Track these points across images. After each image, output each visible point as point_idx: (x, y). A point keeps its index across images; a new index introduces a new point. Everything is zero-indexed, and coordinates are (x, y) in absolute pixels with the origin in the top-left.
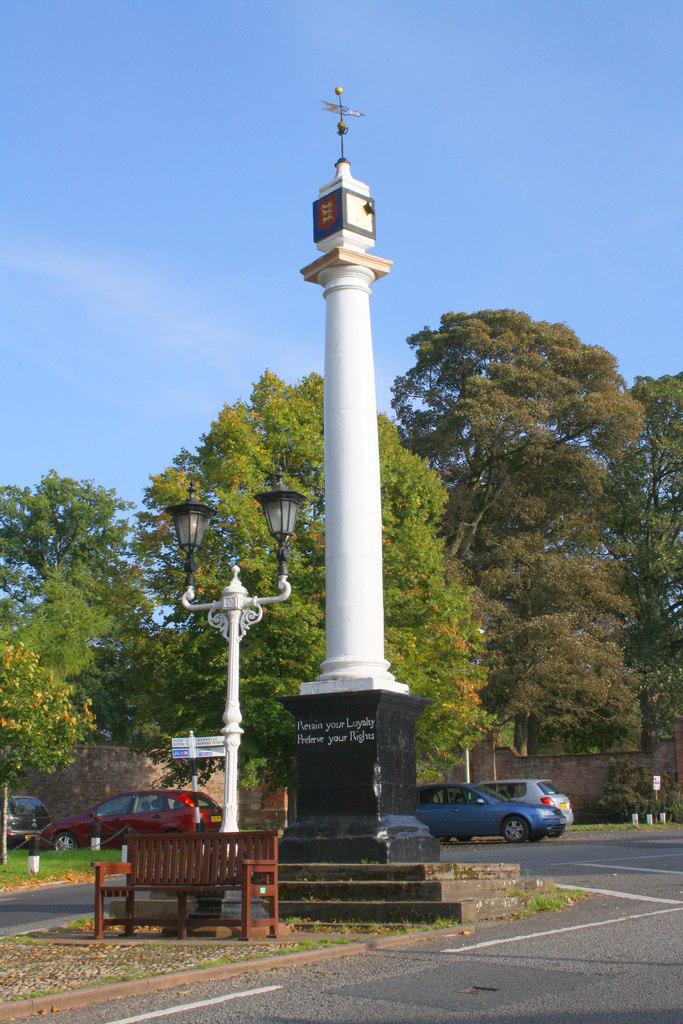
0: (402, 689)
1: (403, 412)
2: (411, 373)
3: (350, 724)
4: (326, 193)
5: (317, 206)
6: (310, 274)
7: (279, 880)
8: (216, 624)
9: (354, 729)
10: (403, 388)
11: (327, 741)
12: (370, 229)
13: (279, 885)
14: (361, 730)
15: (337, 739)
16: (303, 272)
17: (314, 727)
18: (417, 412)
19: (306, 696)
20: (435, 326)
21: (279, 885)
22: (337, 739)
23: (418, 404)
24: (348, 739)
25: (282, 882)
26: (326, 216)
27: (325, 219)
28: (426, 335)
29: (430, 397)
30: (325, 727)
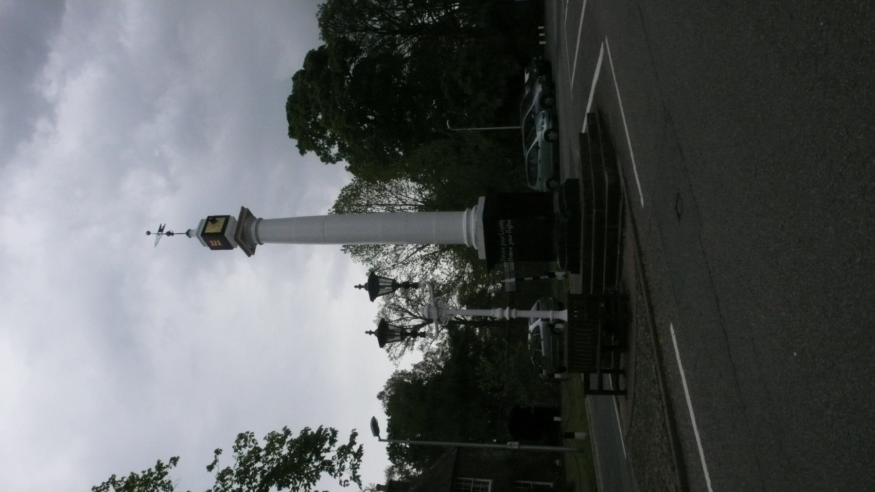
0: (482, 200)
1: (339, 158)
2: (318, 154)
3: (502, 233)
4: (205, 243)
5: (212, 248)
6: (250, 251)
7: (519, 131)
8: (446, 321)
9: (505, 231)
10: (327, 159)
11: (511, 246)
12: (206, 232)
13: (519, 124)
14: (506, 226)
15: (510, 240)
16: (249, 255)
17: (504, 252)
18: (339, 150)
19: (486, 255)
20: (295, 142)
21: (519, 124)
22: (510, 240)
23: (335, 150)
24: (510, 234)
25: (518, 127)
26: (218, 243)
27: (220, 244)
28: (299, 146)
29: (331, 143)
30: (504, 246)
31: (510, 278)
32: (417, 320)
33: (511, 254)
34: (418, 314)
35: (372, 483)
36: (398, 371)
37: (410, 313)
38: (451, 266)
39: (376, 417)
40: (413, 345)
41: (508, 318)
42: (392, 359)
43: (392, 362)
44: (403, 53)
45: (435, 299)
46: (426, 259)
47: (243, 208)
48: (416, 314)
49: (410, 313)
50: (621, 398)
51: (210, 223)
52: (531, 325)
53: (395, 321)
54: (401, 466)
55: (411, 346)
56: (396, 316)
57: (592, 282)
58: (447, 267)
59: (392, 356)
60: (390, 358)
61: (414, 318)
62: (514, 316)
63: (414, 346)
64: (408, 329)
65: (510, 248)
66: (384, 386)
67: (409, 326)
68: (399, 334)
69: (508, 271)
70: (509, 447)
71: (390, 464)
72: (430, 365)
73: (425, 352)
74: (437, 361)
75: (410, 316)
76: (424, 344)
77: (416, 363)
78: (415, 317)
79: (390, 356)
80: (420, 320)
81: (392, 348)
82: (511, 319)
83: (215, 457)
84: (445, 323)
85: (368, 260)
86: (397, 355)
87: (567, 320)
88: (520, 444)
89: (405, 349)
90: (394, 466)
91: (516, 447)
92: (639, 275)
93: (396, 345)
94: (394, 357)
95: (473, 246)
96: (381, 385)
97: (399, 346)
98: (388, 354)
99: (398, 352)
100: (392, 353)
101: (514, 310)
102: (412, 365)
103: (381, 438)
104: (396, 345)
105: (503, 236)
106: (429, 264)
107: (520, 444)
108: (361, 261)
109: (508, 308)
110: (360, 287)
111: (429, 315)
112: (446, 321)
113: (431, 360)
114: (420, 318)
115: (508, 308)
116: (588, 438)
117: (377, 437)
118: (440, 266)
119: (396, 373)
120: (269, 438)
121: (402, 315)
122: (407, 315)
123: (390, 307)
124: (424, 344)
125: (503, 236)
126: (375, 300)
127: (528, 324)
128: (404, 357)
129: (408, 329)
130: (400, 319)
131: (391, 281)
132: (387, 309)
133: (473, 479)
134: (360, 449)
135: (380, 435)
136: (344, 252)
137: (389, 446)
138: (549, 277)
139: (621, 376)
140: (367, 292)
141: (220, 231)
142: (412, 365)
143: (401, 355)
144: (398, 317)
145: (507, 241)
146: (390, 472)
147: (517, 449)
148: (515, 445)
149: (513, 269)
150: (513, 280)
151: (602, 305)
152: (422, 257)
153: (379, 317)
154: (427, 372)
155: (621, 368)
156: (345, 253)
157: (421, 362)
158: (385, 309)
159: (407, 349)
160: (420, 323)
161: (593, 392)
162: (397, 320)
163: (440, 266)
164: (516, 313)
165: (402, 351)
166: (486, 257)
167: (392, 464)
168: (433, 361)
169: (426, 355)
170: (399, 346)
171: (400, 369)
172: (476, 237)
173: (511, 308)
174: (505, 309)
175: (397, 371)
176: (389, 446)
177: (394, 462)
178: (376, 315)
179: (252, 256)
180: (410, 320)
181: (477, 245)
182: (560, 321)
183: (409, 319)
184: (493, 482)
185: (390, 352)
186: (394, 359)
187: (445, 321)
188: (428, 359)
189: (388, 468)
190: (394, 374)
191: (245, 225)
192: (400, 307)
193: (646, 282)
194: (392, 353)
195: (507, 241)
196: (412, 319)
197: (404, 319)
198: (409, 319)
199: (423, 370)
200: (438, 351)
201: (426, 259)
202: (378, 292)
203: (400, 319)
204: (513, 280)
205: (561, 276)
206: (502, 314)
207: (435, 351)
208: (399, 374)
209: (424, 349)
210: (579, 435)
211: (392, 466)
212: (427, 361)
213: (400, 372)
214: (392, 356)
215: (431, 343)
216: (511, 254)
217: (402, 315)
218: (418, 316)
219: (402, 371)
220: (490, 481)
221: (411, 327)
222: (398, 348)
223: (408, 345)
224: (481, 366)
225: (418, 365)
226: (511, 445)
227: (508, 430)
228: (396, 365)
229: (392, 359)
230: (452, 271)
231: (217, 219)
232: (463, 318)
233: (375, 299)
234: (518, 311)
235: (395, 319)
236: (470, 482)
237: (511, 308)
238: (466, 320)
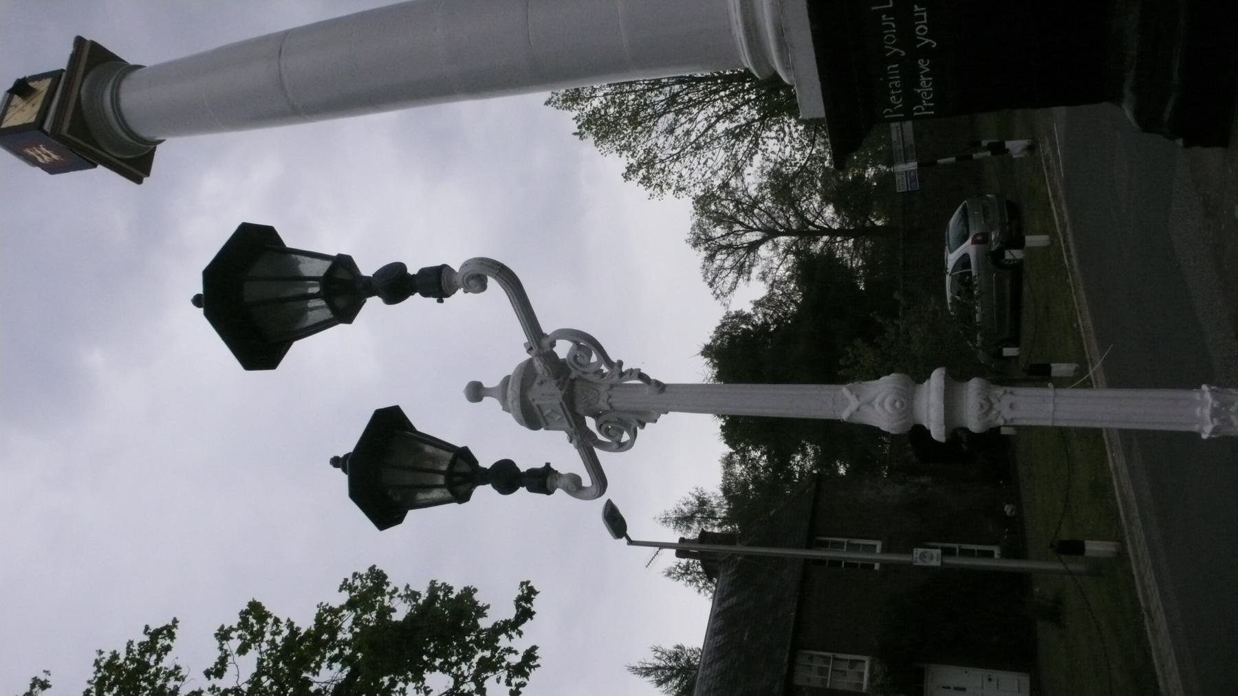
11: (926, 52)
13: (844, 542)
15: (921, 27)
22: (921, 27)
30: (896, 58)
31: (906, 162)
32: (754, 233)
33: (925, 86)
34: (755, 224)
35: (699, 488)
36: (731, 312)
37: (742, 224)
38: (786, 146)
39: (615, 502)
40: (750, 273)
41: (937, 432)
42: (718, 297)
43: (718, 302)
46: (735, 135)
47: (79, 42)
48: (751, 224)
49: (742, 224)
51: (17, 100)
52: (951, 252)
53: (719, 238)
54: (743, 453)
55: (747, 275)
56: (720, 230)
58: (776, 149)
59: (718, 292)
60: (715, 296)
61: (748, 232)
62: (973, 423)
63: (752, 274)
64: (741, 248)
65: (921, 62)
66: (711, 337)
67: (742, 244)
68: (441, 480)
69: (901, 147)
70: (920, 563)
71: (727, 450)
72: (781, 301)
73: (770, 282)
74: (789, 294)
75: (742, 229)
76: (767, 270)
77: (758, 298)
79: (714, 292)
80: (758, 233)
81: (717, 280)
82: (957, 434)
83: (221, 648)
85: (627, 147)
86: (726, 290)
88: (947, 552)
89: (737, 280)
90: (734, 453)
91: (935, 563)
93: (724, 275)
94: (722, 294)
95: (776, 74)
96: (706, 335)
97: (727, 276)
98: (711, 290)
99: (728, 285)
100: (717, 288)
101: (974, 386)
102: (751, 302)
103: (633, 539)
104: (724, 275)
105: (889, 12)
106: (742, 147)
108: (615, 151)
109: (937, 377)
113: (781, 293)
114: (759, 230)
116: (1121, 555)
117: (624, 540)
118: (763, 147)
119: (728, 316)
120: (822, 191)
121: (730, 228)
122: (737, 227)
123: (709, 217)
124: (767, 270)
125: (889, 12)
127: (943, 250)
128: (736, 292)
129: (741, 248)
130: (728, 234)
132: (704, 220)
133: (845, 540)
134: (530, 656)
135: (628, 532)
136: (578, 137)
137: (724, 424)
138: (992, 154)
141: (32, 120)
142: (751, 302)
143: (731, 290)
144: (723, 232)
145: (906, 36)
146: (728, 462)
147: (937, 567)
148: (932, 558)
149: (912, 142)
150: (912, 165)
152: (728, 133)
153: (695, 234)
154: (775, 312)
156: (581, 138)
157: (766, 296)
158: (702, 221)
159: (741, 280)
160: (759, 238)
162: (722, 236)
163: (763, 147)
164: (987, 406)
165: (733, 283)
166: (826, 111)
167: (732, 450)
168: (784, 294)
169: (772, 286)
170: (727, 276)
171: (733, 309)
172: (780, 32)
173: (956, 377)
174: (921, 377)
175: (728, 313)
176: (724, 424)
177: (732, 446)
178: (689, 231)
179: (146, 180)
180: (742, 234)
181: (787, 68)
183: (741, 232)
184: (883, 545)
185: (715, 286)
186: (722, 297)
188: (776, 291)
189: (724, 456)
190: (724, 318)
191: (83, 92)
192: (725, 215)
193: (903, 136)
194: (717, 288)
195: (906, 36)
196: (746, 232)
197: (733, 233)
198: (741, 232)
199: (768, 309)
200: (791, 277)
201: (735, 135)
203: (728, 234)
204: (912, 165)
205: (1020, 149)
206: (907, 404)
207: (785, 278)
208: (733, 318)
209: (768, 279)
210: (1094, 547)
211: (730, 453)
212: (774, 294)
213: (734, 313)
214: (718, 292)
215: (778, 269)
216: (925, 86)
217: (730, 228)
218: (755, 227)
219: (736, 312)
221: (745, 245)
222: (726, 279)
223: (742, 273)
224: (850, 355)
225: (760, 301)
226: (923, 556)
227: (909, 445)
228: (724, 305)
229: (718, 297)
230: (787, 154)
231: (31, 84)
232: (826, 226)
234: (999, 391)
235: (719, 235)
237: (956, 377)
238: (830, 228)
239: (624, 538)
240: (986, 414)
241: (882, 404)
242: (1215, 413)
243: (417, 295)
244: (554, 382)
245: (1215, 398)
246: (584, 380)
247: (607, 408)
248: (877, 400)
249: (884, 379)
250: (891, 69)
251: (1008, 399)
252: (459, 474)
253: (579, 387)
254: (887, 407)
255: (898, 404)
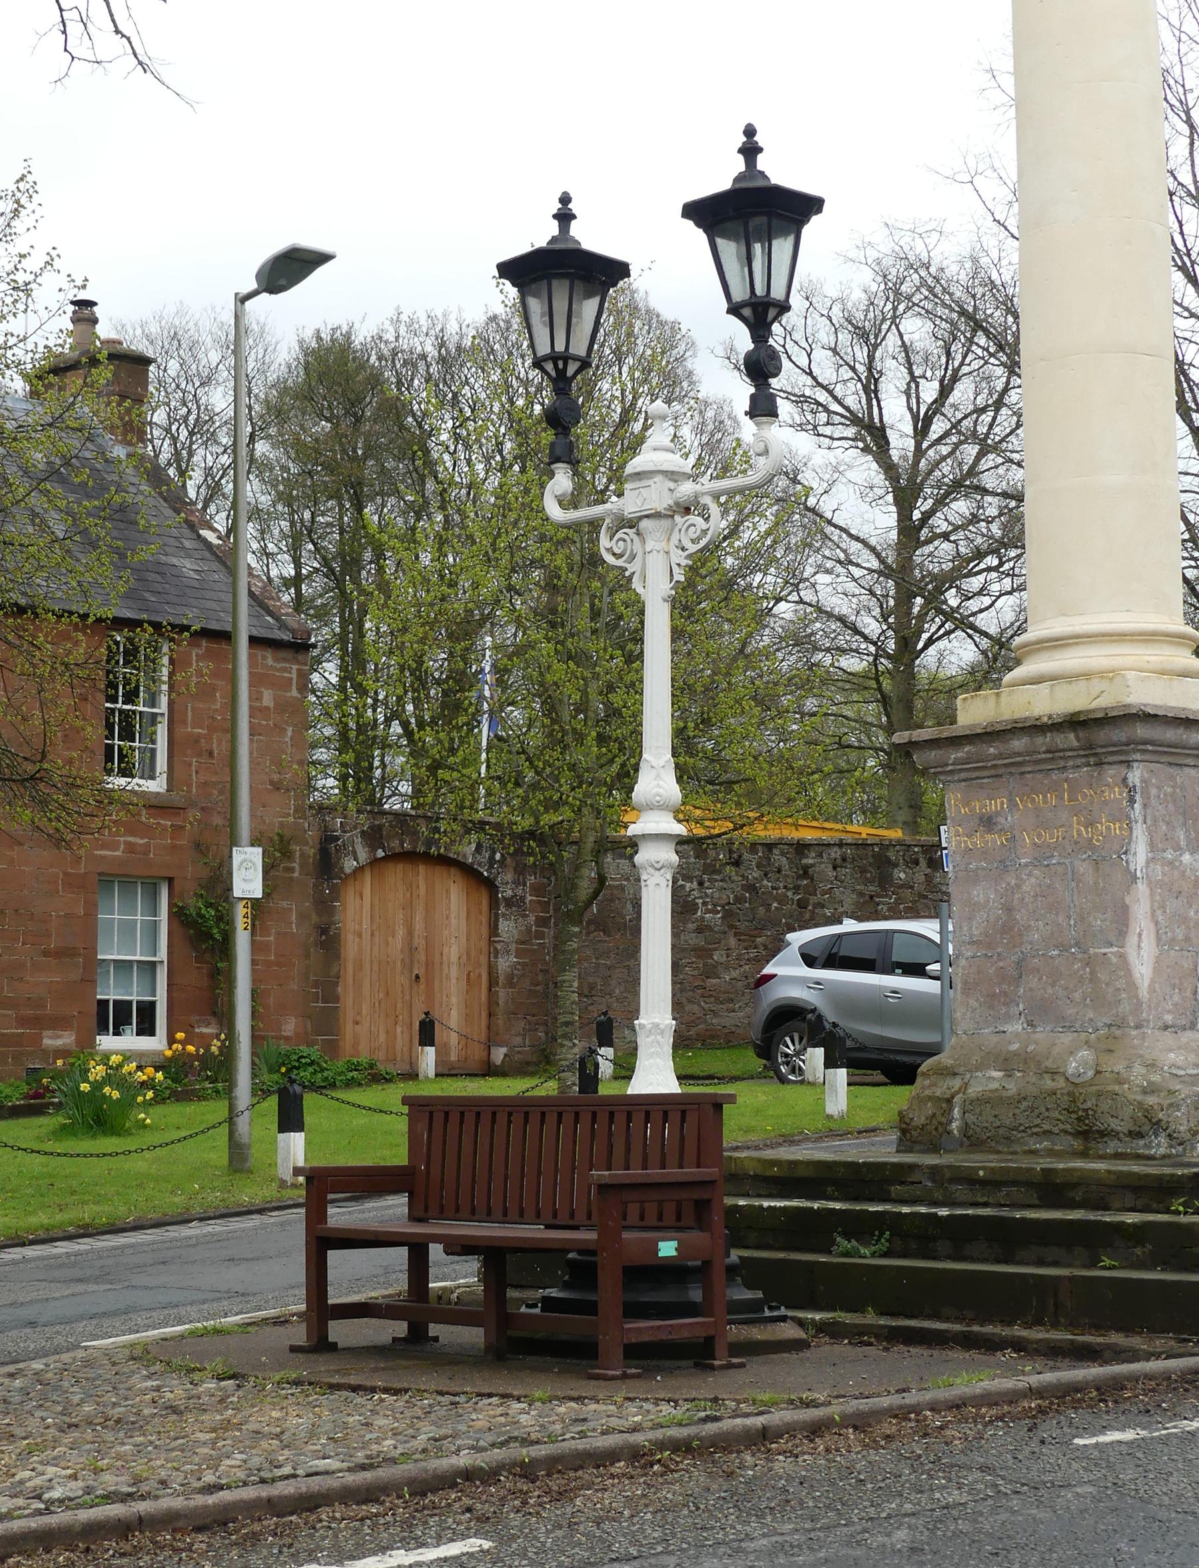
8: (617, 556)
32: (910, 444)
40: (801, 427)
44: (751, 225)
45: (707, 500)
50: (299, 1334)
57: (838, 1206)
61: (915, 417)
68: (560, 347)
78: (922, 427)
84: (609, 550)
87: (629, 1092)
92: (761, 1413)
107: (255, 903)
110: (750, 151)
111: (639, 475)
112: (617, 556)
114: (919, 452)
115: (680, 829)
117: (253, 285)
126: (690, 224)
131: (777, 293)
139: (400, 1328)
140: (724, 184)
151: (668, 1249)
155: (434, 1329)
160: (895, 455)
161: (316, 1211)
173: (681, 842)
182: (625, 1070)
187: (617, 551)
202: (723, 236)
220: (156, 786)
232: (920, 645)
233: (698, 225)
234: (669, 876)
236: (153, 702)
237: (681, 842)
239: (253, 285)
240: (652, 866)
241: (658, 786)
242: (657, 1026)
243: (753, 390)
244: (671, 502)
245: (667, 1026)
246: (672, 530)
247: (648, 550)
248: (661, 782)
249: (677, 788)
250: (1002, 803)
251: (663, 883)
252: (565, 365)
253: (665, 523)
254: (655, 790)
255: (658, 798)
